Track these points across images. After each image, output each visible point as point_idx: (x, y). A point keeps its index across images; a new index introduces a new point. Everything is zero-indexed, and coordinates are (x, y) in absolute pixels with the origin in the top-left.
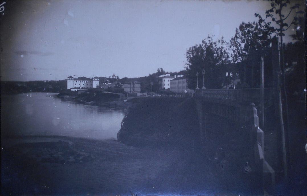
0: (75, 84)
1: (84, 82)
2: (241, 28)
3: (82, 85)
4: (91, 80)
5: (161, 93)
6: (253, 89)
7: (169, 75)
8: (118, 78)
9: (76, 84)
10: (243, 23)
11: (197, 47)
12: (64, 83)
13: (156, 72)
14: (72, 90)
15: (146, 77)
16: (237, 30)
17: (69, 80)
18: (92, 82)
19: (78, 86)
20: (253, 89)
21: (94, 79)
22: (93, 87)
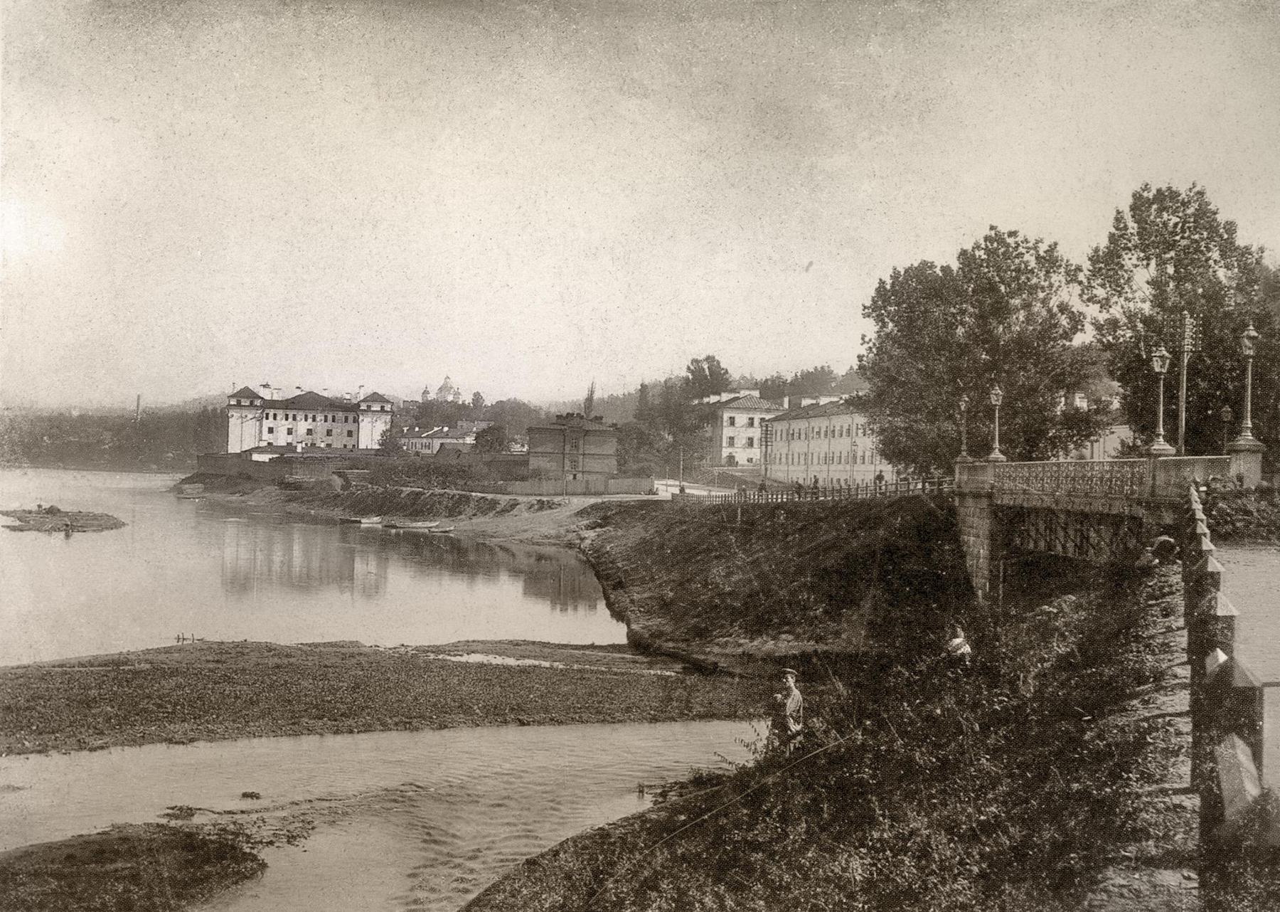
0: (265, 430)
1: (314, 420)
2: (1139, 203)
3: (287, 432)
4: (348, 410)
5: (725, 480)
6: (438, 491)
7: (756, 394)
8: (477, 397)
9: (271, 430)
10: (1146, 188)
11: (1250, 799)
12: (206, 424)
13: (680, 370)
14: (256, 457)
15: (617, 398)
16: (1119, 219)
17: (239, 405)
18: (356, 421)
19: (282, 439)
20: (438, 491)
21: (363, 407)
22: (362, 446)
